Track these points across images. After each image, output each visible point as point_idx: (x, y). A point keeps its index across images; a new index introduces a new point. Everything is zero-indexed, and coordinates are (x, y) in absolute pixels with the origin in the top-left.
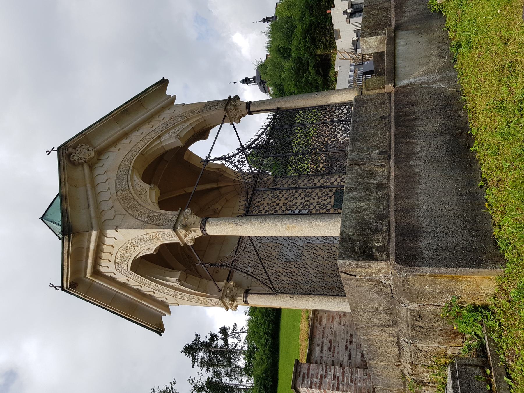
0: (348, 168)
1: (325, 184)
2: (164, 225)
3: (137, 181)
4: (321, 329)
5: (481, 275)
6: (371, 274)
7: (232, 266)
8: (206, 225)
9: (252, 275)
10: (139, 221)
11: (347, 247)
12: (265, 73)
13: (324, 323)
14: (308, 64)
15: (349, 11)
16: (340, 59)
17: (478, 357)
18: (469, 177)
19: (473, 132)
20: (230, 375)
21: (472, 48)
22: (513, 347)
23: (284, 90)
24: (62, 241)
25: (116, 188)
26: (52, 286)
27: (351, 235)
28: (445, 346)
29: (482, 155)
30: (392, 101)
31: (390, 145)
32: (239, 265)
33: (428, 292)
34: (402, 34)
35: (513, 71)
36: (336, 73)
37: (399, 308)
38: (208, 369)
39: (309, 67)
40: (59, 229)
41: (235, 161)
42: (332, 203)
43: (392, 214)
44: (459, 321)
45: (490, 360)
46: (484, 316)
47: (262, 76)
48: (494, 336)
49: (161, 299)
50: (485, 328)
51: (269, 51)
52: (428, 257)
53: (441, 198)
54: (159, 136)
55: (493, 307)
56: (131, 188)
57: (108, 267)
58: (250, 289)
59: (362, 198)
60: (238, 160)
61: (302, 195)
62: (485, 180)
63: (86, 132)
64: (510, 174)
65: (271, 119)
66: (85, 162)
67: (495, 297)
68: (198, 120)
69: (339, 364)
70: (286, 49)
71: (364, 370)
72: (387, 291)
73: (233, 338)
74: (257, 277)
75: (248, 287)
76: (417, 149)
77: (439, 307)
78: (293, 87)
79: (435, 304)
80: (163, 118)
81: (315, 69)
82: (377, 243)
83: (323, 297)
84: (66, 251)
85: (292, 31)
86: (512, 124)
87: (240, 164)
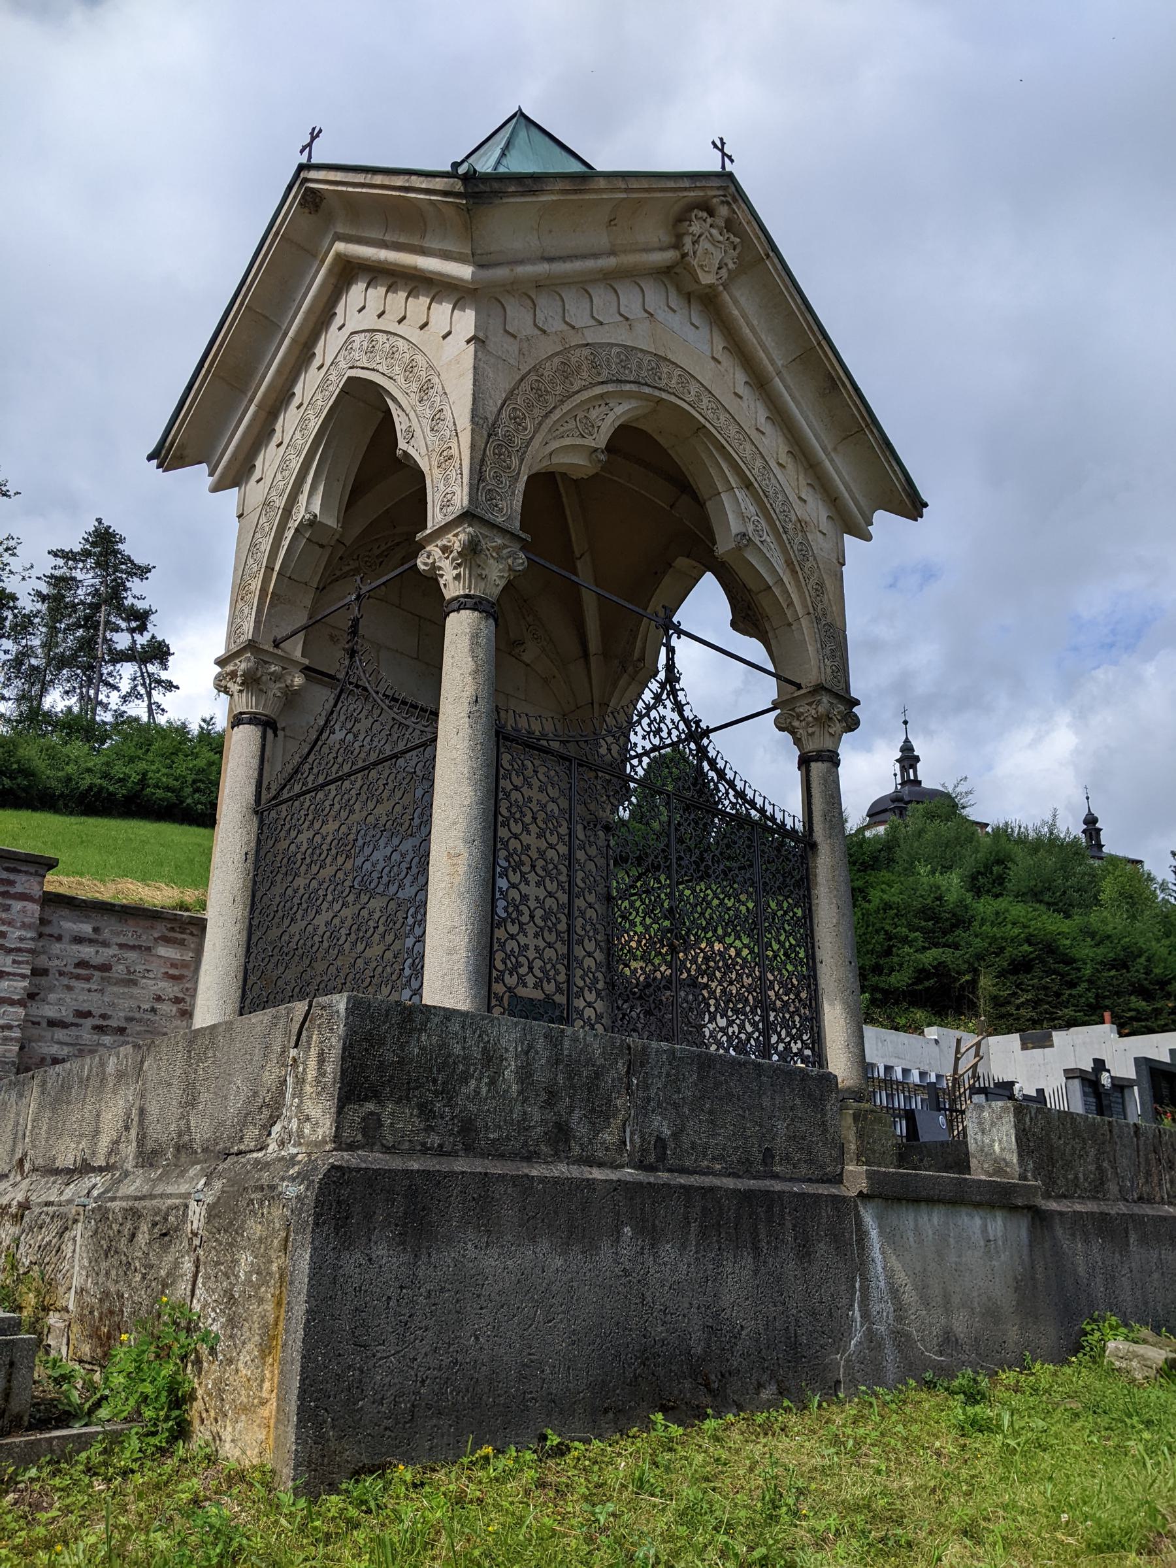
0: (622, 1040)
1: (579, 972)
2: (481, 486)
3: (619, 410)
4: (145, 941)
5: (278, 1421)
6: (299, 1094)
7: (351, 683)
8: (476, 614)
9: (320, 743)
10: (495, 410)
11: (384, 1023)
12: (931, 816)
13: (164, 951)
14: (949, 947)
15: (1105, 1079)
16: (959, 1041)
17: (34, 1405)
18: (575, 1403)
19: (710, 1424)
20: (22, 663)
21: (963, 1435)
22: (57, 1505)
23: (873, 869)
24: (448, 173)
25: (601, 345)
26: (315, 135)
27: (418, 1040)
28: (71, 1307)
29: (639, 1445)
30: (817, 1185)
31: (682, 1171)
32: (351, 705)
33: (236, 1262)
34: (1021, 1229)
35: (884, 1548)
36: (918, 1030)
37: (192, 1172)
38: (42, 597)
39: (941, 950)
40: (485, 164)
41: (660, 708)
42: (522, 992)
43: (478, 1166)
44: (144, 1352)
45: (21, 1436)
46: (155, 1425)
47: (920, 806)
48: (94, 1453)
49: (258, 463)
50: (119, 1427)
51: (997, 830)
52: (341, 1267)
53: (514, 1316)
54: (752, 484)
55: (181, 1452)
56: (598, 390)
57: (364, 308)
58: (276, 735)
59: (527, 1077)
60: (663, 718)
61: (550, 902)
62: (561, 1451)
63: (776, 261)
64: (574, 1522)
65: (783, 822)
66: (684, 256)
67: (209, 1460)
68: (791, 604)
69: (37, 991)
70: (1001, 884)
71: (13, 1063)
72: (246, 1140)
73: (134, 679)
74: (312, 757)
75: (283, 729)
76: (668, 1251)
77: (189, 1293)
78: (881, 899)
79: (200, 1281)
80: (804, 496)
81: (934, 967)
82: (392, 1114)
83: (241, 951)
84: (416, 182)
85: (1056, 904)
86: (725, 1538)
87: (652, 722)
